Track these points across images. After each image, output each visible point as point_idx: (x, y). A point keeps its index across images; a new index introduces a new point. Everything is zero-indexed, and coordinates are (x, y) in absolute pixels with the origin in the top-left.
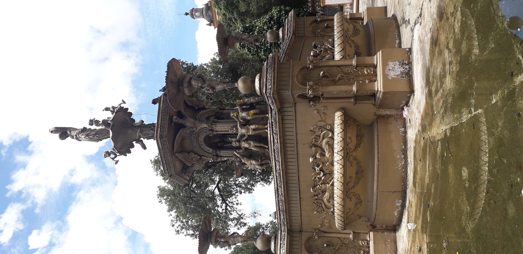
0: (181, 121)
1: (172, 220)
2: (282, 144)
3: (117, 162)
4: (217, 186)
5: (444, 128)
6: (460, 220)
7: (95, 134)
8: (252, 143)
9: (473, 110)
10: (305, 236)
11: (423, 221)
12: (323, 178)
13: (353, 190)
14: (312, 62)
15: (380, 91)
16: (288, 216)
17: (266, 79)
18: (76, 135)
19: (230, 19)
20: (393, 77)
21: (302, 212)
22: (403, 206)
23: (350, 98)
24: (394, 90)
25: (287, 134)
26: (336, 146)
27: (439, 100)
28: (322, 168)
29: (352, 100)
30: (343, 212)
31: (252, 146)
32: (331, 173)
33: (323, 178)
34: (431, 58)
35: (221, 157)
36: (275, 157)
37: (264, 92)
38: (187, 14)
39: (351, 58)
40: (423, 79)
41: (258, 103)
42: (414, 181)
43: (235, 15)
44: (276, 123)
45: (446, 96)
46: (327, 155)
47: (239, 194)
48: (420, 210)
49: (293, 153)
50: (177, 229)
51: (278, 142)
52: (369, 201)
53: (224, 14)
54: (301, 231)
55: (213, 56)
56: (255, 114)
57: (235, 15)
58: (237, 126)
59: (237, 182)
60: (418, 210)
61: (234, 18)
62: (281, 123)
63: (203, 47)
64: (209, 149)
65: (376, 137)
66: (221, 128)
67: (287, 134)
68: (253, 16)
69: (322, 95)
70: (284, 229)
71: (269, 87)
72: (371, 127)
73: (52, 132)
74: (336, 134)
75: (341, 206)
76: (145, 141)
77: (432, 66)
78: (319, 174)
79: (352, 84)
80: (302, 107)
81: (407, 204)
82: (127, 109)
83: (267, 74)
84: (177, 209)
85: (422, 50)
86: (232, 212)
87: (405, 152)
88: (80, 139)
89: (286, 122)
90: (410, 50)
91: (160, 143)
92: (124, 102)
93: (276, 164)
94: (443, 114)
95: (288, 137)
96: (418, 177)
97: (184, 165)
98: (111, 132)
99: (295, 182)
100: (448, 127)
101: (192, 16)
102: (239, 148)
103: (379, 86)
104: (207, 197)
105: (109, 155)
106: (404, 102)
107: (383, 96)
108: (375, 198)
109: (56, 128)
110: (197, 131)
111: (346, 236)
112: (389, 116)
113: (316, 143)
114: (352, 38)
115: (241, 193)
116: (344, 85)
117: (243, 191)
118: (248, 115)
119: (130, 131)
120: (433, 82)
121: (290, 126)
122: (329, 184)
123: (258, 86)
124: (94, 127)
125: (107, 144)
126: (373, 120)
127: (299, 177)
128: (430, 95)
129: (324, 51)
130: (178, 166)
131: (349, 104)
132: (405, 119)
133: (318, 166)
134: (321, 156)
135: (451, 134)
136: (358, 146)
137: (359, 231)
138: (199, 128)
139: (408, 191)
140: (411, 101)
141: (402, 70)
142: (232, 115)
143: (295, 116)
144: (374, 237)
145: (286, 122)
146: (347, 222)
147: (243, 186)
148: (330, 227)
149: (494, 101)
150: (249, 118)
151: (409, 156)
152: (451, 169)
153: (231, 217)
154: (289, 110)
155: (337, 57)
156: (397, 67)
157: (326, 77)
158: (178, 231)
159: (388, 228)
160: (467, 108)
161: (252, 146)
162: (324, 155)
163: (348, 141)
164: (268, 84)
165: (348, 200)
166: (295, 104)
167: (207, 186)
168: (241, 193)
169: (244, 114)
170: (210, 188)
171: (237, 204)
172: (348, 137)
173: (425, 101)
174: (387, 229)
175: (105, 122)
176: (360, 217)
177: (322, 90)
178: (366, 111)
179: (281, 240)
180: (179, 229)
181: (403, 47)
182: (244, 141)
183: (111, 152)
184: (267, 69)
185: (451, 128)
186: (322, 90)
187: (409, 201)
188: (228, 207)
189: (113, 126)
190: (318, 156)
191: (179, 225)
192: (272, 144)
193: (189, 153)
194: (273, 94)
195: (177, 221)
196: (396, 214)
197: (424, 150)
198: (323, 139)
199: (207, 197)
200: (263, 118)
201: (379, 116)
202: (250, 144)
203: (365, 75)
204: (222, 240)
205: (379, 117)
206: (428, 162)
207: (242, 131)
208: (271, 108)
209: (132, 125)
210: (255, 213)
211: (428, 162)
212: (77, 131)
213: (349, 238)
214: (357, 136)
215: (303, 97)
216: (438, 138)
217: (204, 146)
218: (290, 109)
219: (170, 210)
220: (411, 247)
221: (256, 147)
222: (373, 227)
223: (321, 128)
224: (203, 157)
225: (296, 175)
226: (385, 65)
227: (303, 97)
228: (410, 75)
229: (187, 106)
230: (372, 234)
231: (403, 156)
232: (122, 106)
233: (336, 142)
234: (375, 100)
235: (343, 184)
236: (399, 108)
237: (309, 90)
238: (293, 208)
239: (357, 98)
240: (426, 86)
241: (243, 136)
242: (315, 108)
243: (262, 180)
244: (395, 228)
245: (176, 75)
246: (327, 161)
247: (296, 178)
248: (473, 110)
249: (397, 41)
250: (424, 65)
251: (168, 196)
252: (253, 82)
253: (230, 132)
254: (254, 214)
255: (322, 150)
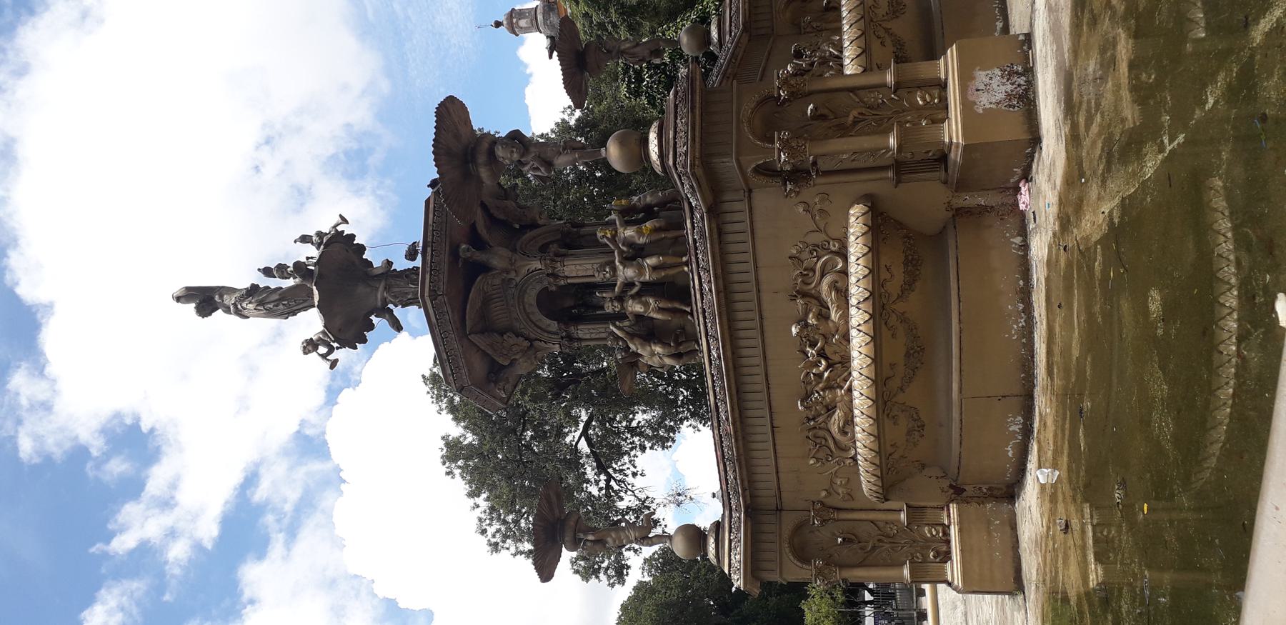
0: (480, 256)
1: (480, 520)
2: (722, 294)
3: (334, 364)
4: (585, 433)
5: (1106, 208)
6: (1148, 424)
7: (280, 300)
8: (651, 301)
9: (1166, 141)
10: (789, 521)
11: (1070, 455)
12: (826, 374)
13: (901, 398)
14: (785, 82)
15: (958, 144)
16: (745, 473)
17: (675, 132)
18: (235, 305)
19: (601, 26)
20: (988, 106)
21: (781, 461)
22: (1027, 432)
23: (884, 168)
24: (990, 140)
25: (736, 277)
26: (853, 290)
27: (1094, 143)
28: (822, 349)
29: (890, 174)
30: (879, 453)
31: (651, 308)
32: (846, 361)
33: (826, 374)
34: (1073, 44)
35: (580, 340)
36: (706, 327)
37: (671, 162)
38: (498, 24)
39: (882, 68)
40: (1059, 101)
41: (663, 205)
42: (1048, 361)
43: (613, 15)
44: (705, 243)
45: (1109, 125)
46: (834, 315)
47: (639, 453)
48: (1063, 431)
49: (750, 315)
50: (493, 540)
51: (710, 290)
52: (941, 425)
53: (586, 15)
54: (779, 510)
55: (562, 116)
56: (656, 230)
57: (614, 16)
58: (613, 262)
59: (634, 424)
60: (1059, 432)
61: (611, 22)
62: (716, 241)
63: (539, 99)
64: (549, 321)
65: (952, 262)
66: (577, 269)
67: (735, 267)
68: (657, 14)
69: (814, 163)
70: (738, 505)
71: (682, 149)
72: (938, 239)
73: (178, 299)
74: (852, 259)
75: (872, 438)
76: (398, 311)
77: (1075, 64)
78: (817, 364)
79: (902, 564)
80: (767, 198)
81: (1036, 425)
82: (352, 237)
83: (676, 118)
84: (490, 491)
85: (1055, 29)
86: (622, 494)
87: (1025, 295)
88: (245, 312)
89: (731, 238)
90: (1029, 38)
91: (431, 311)
92: (345, 221)
93: (711, 351)
94: (1103, 174)
95: (736, 277)
96: (1057, 350)
97: (493, 362)
98: (316, 292)
99: (758, 387)
100: (1117, 200)
101: (513, 29)
102: (621, 316)
103: (953, 131)
104: (560, 461)
105: (315, 348)
106: (1018, 170)
107: (963, 157)
108: (956, 415)
109: (187, 288)
110: (518, 279)
111: (890, 516)
112: (985, 209)
113: (806, 288)
114: (884, 25)
115: (643, 449)
116: (868, 134)
117: (648, 445)
118: (640, 233)
119: (361, 289)
120: (1081, 103)
121: (741, 247)
122: (842, 388)
123: (656, 149)
124: (274, 283)
125: (311, 322)
126: (941, 221)
127: (767, 375)
128: (1074, 140)
129: (820, 64)
130: (479, 366)
131: (881, 184)
132: (1022, 215)
133: (813, 345)
134: (818, 319)
135: (1121, 217)
136: (908, 287)
137: (922, 504)
138: (524, 271)
139: (1038, 392)
140: (1034, 167)
141: (1009, 87)
142: (599, 234)
143: (752, 222)
144: (959, 515)
145: (731, 238)
146: (889, 484)
147: (649, 432)
148: (850, 496)
149: (1211, 101)
150: (642, 240)
151: (1035, 305)
152: (1125, 306)
153: (621, 505)
154: (736, 208)
155: (850, 68)
156: (995, 82)
157: (823, 117)
158: (496, 544)
159: (995, 492)
160: (1154, 140)
161: (651, 308)
162: (827, 317)
163: (884, 275)
164: (680, 143)
165: (888, 423)
166: (750, 191)
167: (560, 434)
168: (643, 449)
169: (630, 232)
170: (568, 439)
171: (634, 474)
172: (883, 267)
173: (1063, 155)
174: (991, 496)
175: (300, 268)
176: (923, 466)
177: (811, 152)
178: (926, 199)
179: (730, 532)
180: (498, 539)
181: (1012, 33)
182: (633, 297)
183: (320, 339)
184: (676, 106)
185: (1123, 204)
186: (811, 152)
187: (1041, 414)
188: (613, 483)
189: (321, 276)
190: (812, 320)
191: (498, 531)
192: (698, 296)
193: (502, 334)
194: (692, 166)
195: (492, 519)
196: (1010, 454)
197: (1068, 278)
198: (823, 276)
199: (560, 461)
200: (676, 238)
201: (957, 210)
202: (646, 305)
203: (919, 108)
204: (591, 537)
205: (960, 214)
206: (1076, 305)
207: (626, 273)
208: (690, 204)
209: (366, 274)
210: (679, 495)
211: (1076, 305)
212: (237, 295)
213: (899, 521)
214: (906, 264)
215: (768, 171)
216: (1096, 237)
217: (538, 316)
218: (738, 206)
219: (472, 494)
220: (1048, 528)
221: (661, 310)
222: (957, 493)
223: (817, 249)
224: (537, 343)
225: (760, 370)
226: (966, 78)
227: (768, 171)
228: (1028, 99)
229: (492, 220)
230: (953, 508)
231: (1021, 306)
232: (340, 228)
233: (853, 279)
234: (946, 170)
235: (875, 382)
236: (1008, 189)
237: (780, 150)
238: (755, 454)
239: (902, 168)
240: (1065, 118)
241: (629, 285)
242: (800, 199)
243: (693, 415)
244: (1011, 492)
245: (457, 136)
246: (833, 330)
247: (761, 378)
248: (1166, 141)
249: (1000, 25)
250: (1059, 68)
251: (467, 458)
252: (645, 141)
253: (598, 278)
254: (679, 498)
255: (822, 305)
